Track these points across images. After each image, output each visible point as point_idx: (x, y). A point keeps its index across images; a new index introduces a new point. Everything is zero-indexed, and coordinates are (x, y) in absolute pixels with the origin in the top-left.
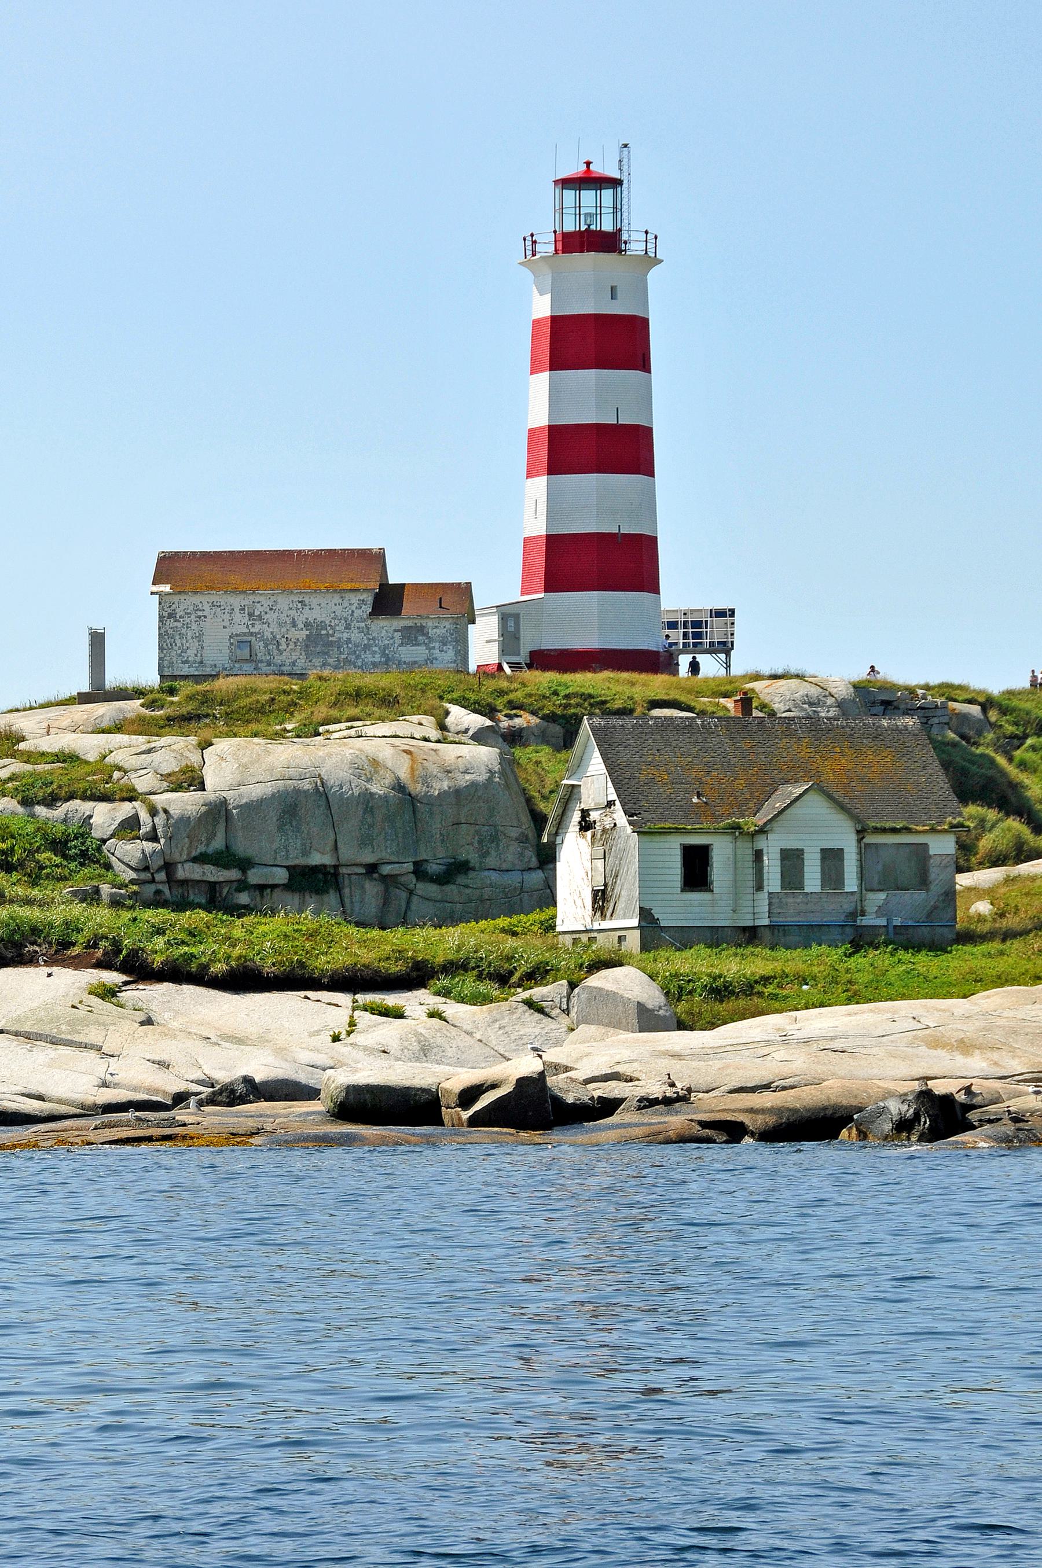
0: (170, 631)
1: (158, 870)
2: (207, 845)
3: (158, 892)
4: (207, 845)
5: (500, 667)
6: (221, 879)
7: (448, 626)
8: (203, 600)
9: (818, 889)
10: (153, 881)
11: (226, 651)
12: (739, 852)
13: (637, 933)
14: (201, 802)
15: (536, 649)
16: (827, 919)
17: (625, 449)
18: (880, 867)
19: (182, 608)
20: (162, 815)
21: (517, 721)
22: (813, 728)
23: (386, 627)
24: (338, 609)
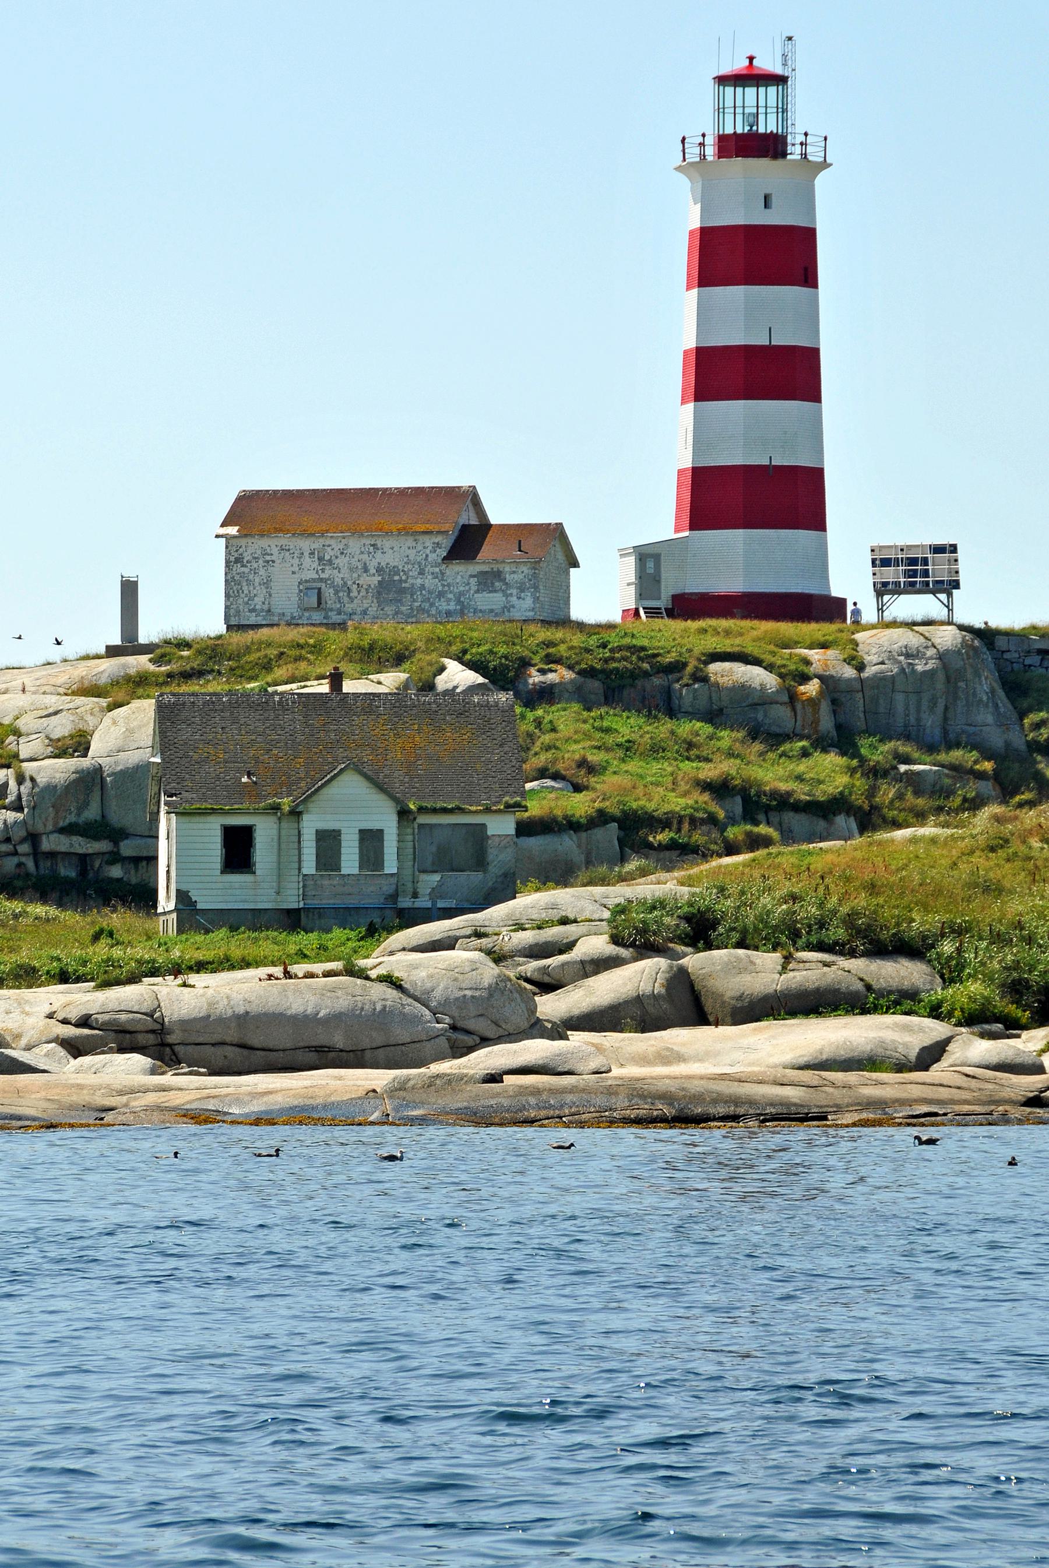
0: (237, 578)
1: (23, 841)
2: (79, 815)
3: (20, 865)
4: (79, 815)
5: (637, 611)
6: (90, 851)
7: (526, 571)
8: (272, 544)
9: (356, 871)
10: (15, 853)
11: (295, 599)
12: (283, 832)
13: (174, 915)
14: (73, 769)
15: (679, 592)
16: (366, 902)
17: (789, 373)
18: (434, 849)
19: (249, 552)
20: (28, 784)
21: (551, 677)
22: (397, 704)
23: (460, 572)
24: (412, 553)
